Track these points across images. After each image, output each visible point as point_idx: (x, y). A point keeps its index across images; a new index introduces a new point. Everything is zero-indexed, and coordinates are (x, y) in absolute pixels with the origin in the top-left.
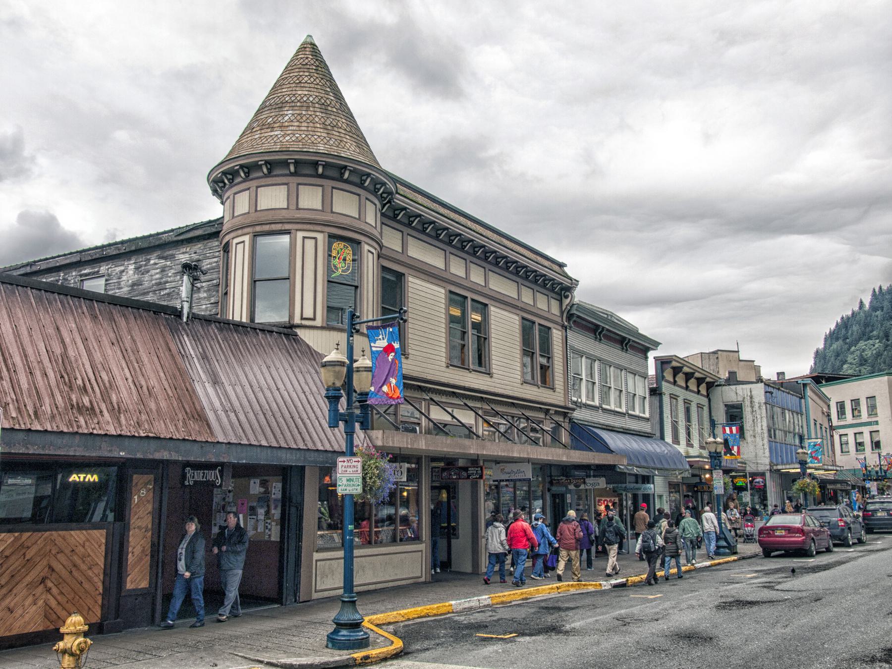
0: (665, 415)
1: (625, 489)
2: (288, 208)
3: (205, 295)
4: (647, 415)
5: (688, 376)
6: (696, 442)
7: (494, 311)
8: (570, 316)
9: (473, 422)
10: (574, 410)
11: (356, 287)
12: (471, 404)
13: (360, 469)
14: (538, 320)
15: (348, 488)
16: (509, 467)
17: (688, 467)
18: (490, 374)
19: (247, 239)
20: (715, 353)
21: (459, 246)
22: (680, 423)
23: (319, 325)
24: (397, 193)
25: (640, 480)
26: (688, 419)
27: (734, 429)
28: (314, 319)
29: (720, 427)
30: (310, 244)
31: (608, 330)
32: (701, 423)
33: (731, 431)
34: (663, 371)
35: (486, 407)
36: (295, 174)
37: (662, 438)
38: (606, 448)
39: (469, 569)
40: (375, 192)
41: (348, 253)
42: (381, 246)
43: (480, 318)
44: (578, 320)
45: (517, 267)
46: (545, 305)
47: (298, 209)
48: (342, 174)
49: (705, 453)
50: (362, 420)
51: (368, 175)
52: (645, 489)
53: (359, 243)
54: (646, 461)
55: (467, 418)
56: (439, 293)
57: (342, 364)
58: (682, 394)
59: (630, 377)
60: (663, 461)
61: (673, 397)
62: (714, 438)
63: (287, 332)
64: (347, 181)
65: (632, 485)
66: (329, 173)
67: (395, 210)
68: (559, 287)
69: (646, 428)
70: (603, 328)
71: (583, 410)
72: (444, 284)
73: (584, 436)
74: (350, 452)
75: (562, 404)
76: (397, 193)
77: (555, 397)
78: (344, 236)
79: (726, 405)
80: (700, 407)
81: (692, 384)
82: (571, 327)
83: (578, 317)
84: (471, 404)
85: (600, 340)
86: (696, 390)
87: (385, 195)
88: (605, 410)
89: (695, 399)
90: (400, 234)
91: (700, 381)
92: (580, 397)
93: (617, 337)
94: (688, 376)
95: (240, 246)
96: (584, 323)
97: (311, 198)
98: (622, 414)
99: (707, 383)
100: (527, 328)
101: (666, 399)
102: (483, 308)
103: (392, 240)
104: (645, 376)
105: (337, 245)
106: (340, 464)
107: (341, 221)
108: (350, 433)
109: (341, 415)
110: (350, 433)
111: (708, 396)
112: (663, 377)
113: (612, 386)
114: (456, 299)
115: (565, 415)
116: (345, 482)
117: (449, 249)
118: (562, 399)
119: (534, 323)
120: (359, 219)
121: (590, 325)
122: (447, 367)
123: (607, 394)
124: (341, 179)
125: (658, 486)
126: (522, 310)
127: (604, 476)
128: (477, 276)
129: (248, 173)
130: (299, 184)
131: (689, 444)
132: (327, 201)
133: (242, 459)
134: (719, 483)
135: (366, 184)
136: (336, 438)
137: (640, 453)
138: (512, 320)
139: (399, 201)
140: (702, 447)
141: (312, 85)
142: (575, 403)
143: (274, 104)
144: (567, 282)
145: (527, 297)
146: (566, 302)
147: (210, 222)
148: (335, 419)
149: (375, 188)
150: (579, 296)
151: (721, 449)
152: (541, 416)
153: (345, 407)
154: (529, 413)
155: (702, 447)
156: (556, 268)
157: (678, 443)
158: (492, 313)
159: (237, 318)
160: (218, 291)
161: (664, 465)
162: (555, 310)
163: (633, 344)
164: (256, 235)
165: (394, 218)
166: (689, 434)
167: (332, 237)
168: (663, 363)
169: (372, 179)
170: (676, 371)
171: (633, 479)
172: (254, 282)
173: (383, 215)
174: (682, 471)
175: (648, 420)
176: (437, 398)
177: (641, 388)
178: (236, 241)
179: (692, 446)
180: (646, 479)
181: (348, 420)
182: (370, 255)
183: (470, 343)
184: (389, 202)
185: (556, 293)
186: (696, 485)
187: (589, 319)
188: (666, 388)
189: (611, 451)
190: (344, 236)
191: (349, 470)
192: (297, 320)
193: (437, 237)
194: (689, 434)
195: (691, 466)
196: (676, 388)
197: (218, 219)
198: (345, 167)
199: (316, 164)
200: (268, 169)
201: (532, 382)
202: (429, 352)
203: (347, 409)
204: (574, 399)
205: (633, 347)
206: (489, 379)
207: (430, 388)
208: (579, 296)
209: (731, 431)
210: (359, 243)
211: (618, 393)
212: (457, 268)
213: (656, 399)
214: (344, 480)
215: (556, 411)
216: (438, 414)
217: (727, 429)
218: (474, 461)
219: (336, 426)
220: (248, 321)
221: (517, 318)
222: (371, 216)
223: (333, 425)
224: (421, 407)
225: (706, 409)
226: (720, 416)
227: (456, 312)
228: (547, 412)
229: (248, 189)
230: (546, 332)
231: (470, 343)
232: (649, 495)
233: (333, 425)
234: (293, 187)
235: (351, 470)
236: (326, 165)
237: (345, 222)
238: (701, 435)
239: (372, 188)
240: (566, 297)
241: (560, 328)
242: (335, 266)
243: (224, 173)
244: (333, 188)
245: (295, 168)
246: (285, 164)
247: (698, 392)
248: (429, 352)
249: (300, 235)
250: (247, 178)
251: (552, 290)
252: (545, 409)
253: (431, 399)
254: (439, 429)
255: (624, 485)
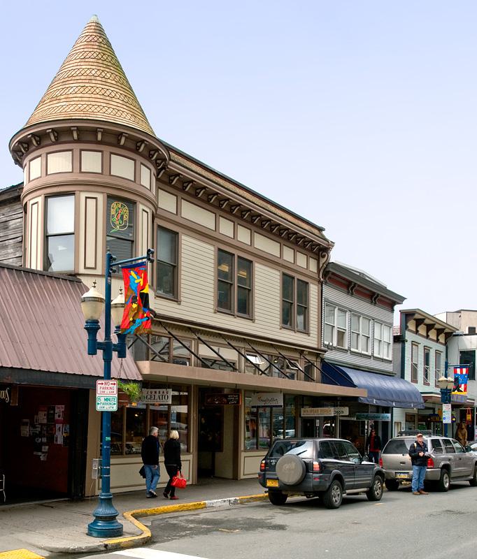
0: (406, 359)
1: (367, 417)
2: (72, 172)
3: (12, 250)
4: (390, 359)
5: (429, 327)
6: (432, 380)
7: (187, 242)
8: (326, 273)
9: (237, 359)
10: (325, 351)
11: (133, 241)
12: (234, 344)
13: (115, 391)
14: (297, 276)
15: (106, 406)
16: (265, 396)
17: (422, 401)
18: (252, 320)
19: (40, 200)
20: (459, 312)
21: (228, 209)
22: (419, 366)
23: (100, 274)
24: (170, 160)
25: (381, 410)
26: (427, 362)
27: (464, 370)
28: (95, 268)
29: (452, 368)
30: (91, 203)
31: (359, 286)
32: (437, 365)
33: (461, 371)
34: (406, 323)
35: (248, 347)
36: (79, 141)
37: (403, 376)
38: (350, 383)
39: (230, 475)
40: (149, 158)
41: (125, 211)
42: (156, 207)
43: (245, 274)
44: (332, 276)
45: (296, 238)
46: (304, 263)
47: (81, 172)
48: (119, 141)
49: (438, 390)
50: (118, 349)
51: (143, 141)
52: (383, 418)
53: (134, 203)
54: (411, 398)
55: (230, 355)
56: (207, 253)
57: (100, 300)
58: (424, 342)
59: (377, 327)
60: (413, 397)
61: (414, 343)
62: (446, 376)
63: (73, 278)
64: (123, 147)
65: (373, 414)
66: (107, 139)
67: (242, 212)
68: (318, 249)
69: (389, 368)
70: (378, 295)
71: (334, 352)
72: (214, 242)
73: (334, 373)
74: (108, 376)
75: (316, 346)
76: (170, 160)
77: (310, 341)
78: (121, 197)
79: (461, 352)
80: (438, 353)
81: (433, 334)
82: (326, 282)
83: (333, 274)
84: (234, 344)
85: (352, 294)
86: (425, 334)
87: (159, 161)
88: (353, 353)
89: (435, 346)
90: (249, 231)
91: (439, 332)
92: (332, 341)
93: (367, 292)
94: (429, 327)
95: (35, 206)
96: (386, 300)
97: (92, 161)
98: (368, 357)
99: (446, 334)
100: (287, 280)
101: (408, 346)
102: (247, 265)
103: (167, 202)
104: (390, 325)
105: (115, 205)
106: (98, 387)
107: (118, 183)
108: (108, 360)
109: (100, 343)
110: (108, 360)
111: (446, 344)
112: (407, 327)
113: (360, 333)
114: (223, 256)
115: (317, 355)
116: (103, 401)
117: (219, 212)
118: (316, 343)
119: (293, 278)
120: (135, 181)
121: (388, 301)
122: (215, 313)
123: (368, 342)
124: (118, 145)
125: (398, 415)
126: (283, 266)
127: (346, 406)
128: (244, 235)
129: (40, 141)
130: (81, 150)
131: (426, 384)
132: (106, 165)
133: (24, 381)
134: (447, 414)
135: (141, 150)
136: (94, 365)
137: (394, 391)
138: (274, 275)
139: (173, 167)
140: (436, 386)
141: (100, 61)
142: (328, 346)
143: (62, 79)
144: (324, 244)
145: (288, 255)
146: (323, 261)
147: (13, 187)
148: (93, 347)
149: (150, 154)
150: (335, 257)
151: (451, 386)
152: (297, 355)
153: (104, 337)
154: (284, 353)
155: (436, 386)
156: (316, 232)
157: (416, 382)
158: (183, 242)
159: (33, 267)
160: (21, 247)
161: (402, 399)
162: (313, 267)
163: (382, 298)
164: (47, 197)
165: (169, 183)
166: (426, 375)
167: (111, 198)
168: (407, 315)
169: (146, 145)
170: (419, 322)
171: (374, 409)
172: (46, 237)
173: (157, 180)
174: (416, 404)
175: (390, 362)
176: (203, 338)
177: (387, 336)
178: (32, 202)
179: (428, 384)
180: (387, 410)
181: (107, 348)
182: (145, 214)
183: (233, 294)
184: (163, 168)
185: (314, 253)
186: (430, 416)
187: (370, 289)
188: (409, 336)
189: (355, 386)
190: (121, 197)
191: (106, 391)
192: (82, 270)
193: (208, 201)
194: (426, 375)
195: (425, 401)
196: (417, 336)
197: (19, 185)
198: (121, 134)
199: (95, 131)
200: (55, 137)
201: (304, 331)
202: (197, 300)
203: (105, 340)
204: (326, 343)
205: (381, 301)
206: (178, 306)
207: (199, 330)
208: (335, 257)
209: (461, 371)
210: (134, 203)
211: (365, 339)
212: (226, 228)
213: (399, 346)
214: (102, 399)
215: (309, 352)
216: (204, 351)
217: (458, 370)
218: (236, 390)
219: (95, 353)
220: (42, 270)
221: (278, 273)
222: (147, 177)
223: (92, 352)
224: (191, 346)
225: (443, 356)
226: (455, 360)
227: (225, 268)
228: (301, 352)
229: (40, 156)
230: (304, 285)
231: (233, 294)
232: (387, 422)
233: (92, 352)
234: (77, 153)
235: (108, 391)
236: (105, 132)
237: (121, 184)
238: (437, 376)
239: (146, 153)
240: (324, 257)
241: (317, 283)
242: (113, 223)
243: (20, 142)
244: (111, 153)
245: (78, 135)
246: (69, 131)
247: (437, 341)
248: (197, 300)
249: (83, 196)
250: (40, 146)
251: (311, 250)
252: (300, 350)
253: (199, 338)
254: (205, 363)
255: (366, 414)
